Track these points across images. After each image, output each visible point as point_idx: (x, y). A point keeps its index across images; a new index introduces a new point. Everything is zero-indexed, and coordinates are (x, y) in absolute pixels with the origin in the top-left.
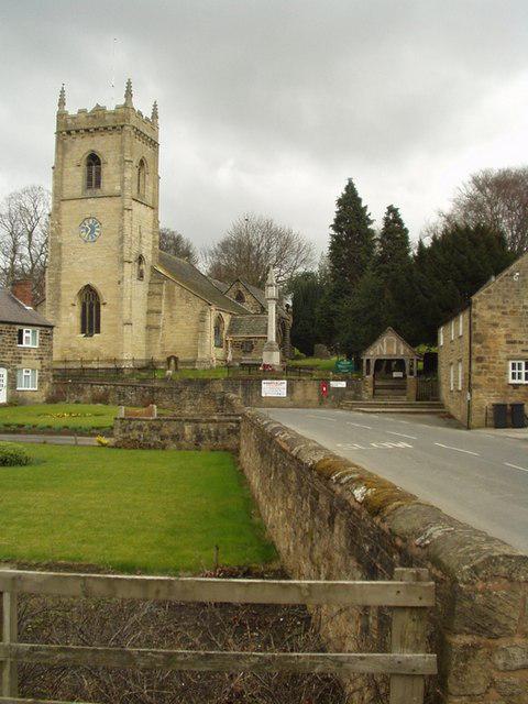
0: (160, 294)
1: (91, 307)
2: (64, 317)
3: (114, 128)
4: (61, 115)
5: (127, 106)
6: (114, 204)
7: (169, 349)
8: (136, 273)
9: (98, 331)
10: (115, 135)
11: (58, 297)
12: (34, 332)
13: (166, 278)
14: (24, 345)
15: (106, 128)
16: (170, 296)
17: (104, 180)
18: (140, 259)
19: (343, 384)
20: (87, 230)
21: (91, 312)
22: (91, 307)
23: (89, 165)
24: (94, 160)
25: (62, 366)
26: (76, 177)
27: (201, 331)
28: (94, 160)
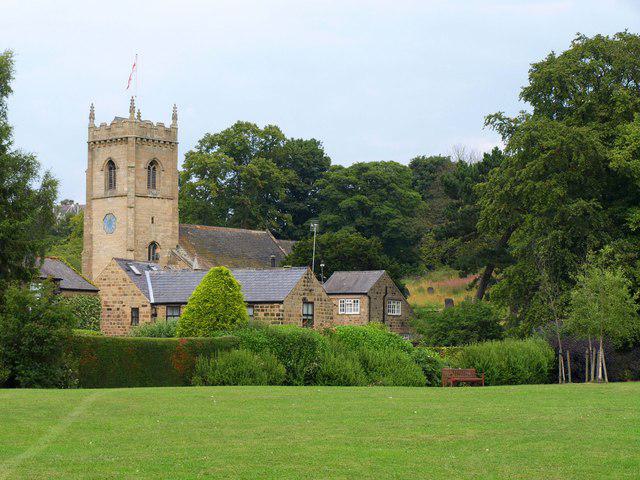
4: (92, 128)
23: (110, 169)
26: (101, 177)
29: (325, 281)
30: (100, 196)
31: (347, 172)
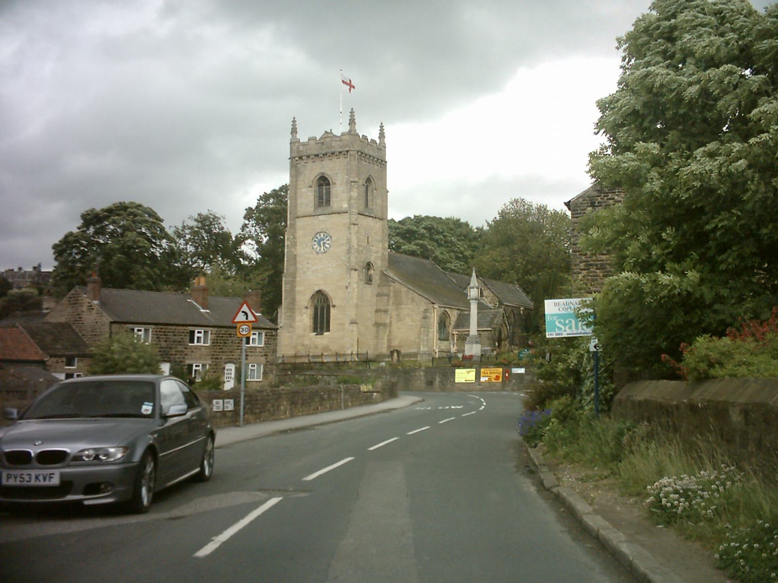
0: (388, 295)
1: (322, 309)
2: (298, 318)
3: (340, 153)
5: (352, 133)
6: (344, 219)
7: (395, 343)
8: (363, 277)
9: (328, 330)
10: (342, 158)
11: (293, 301)
12: (146, 331)
13: (394, 281)
14: (251, 345)
15: (333, 153)
16: (397, 294)
17: (333, 199)
18: (369, 266)
19: (522, 371)
20: (324, 244)
21: (322, 313)
22: (322, 309)
23: (320, 185)
24: (323, 181)
25: (293, 361)
27: (426, 327)
28: (323, 181)
29: (753, 75)
30: (308, 213)
31: (609, 179)
